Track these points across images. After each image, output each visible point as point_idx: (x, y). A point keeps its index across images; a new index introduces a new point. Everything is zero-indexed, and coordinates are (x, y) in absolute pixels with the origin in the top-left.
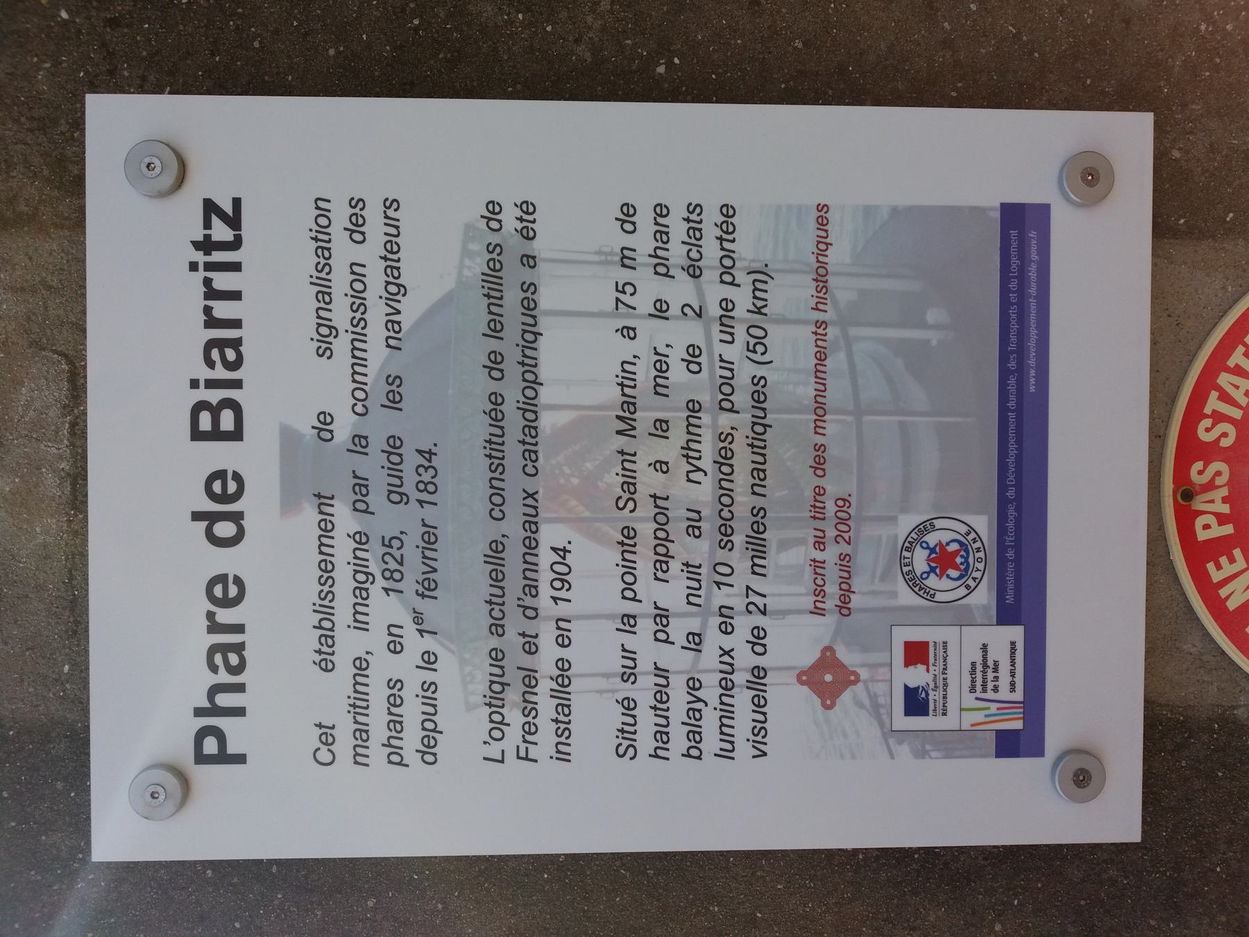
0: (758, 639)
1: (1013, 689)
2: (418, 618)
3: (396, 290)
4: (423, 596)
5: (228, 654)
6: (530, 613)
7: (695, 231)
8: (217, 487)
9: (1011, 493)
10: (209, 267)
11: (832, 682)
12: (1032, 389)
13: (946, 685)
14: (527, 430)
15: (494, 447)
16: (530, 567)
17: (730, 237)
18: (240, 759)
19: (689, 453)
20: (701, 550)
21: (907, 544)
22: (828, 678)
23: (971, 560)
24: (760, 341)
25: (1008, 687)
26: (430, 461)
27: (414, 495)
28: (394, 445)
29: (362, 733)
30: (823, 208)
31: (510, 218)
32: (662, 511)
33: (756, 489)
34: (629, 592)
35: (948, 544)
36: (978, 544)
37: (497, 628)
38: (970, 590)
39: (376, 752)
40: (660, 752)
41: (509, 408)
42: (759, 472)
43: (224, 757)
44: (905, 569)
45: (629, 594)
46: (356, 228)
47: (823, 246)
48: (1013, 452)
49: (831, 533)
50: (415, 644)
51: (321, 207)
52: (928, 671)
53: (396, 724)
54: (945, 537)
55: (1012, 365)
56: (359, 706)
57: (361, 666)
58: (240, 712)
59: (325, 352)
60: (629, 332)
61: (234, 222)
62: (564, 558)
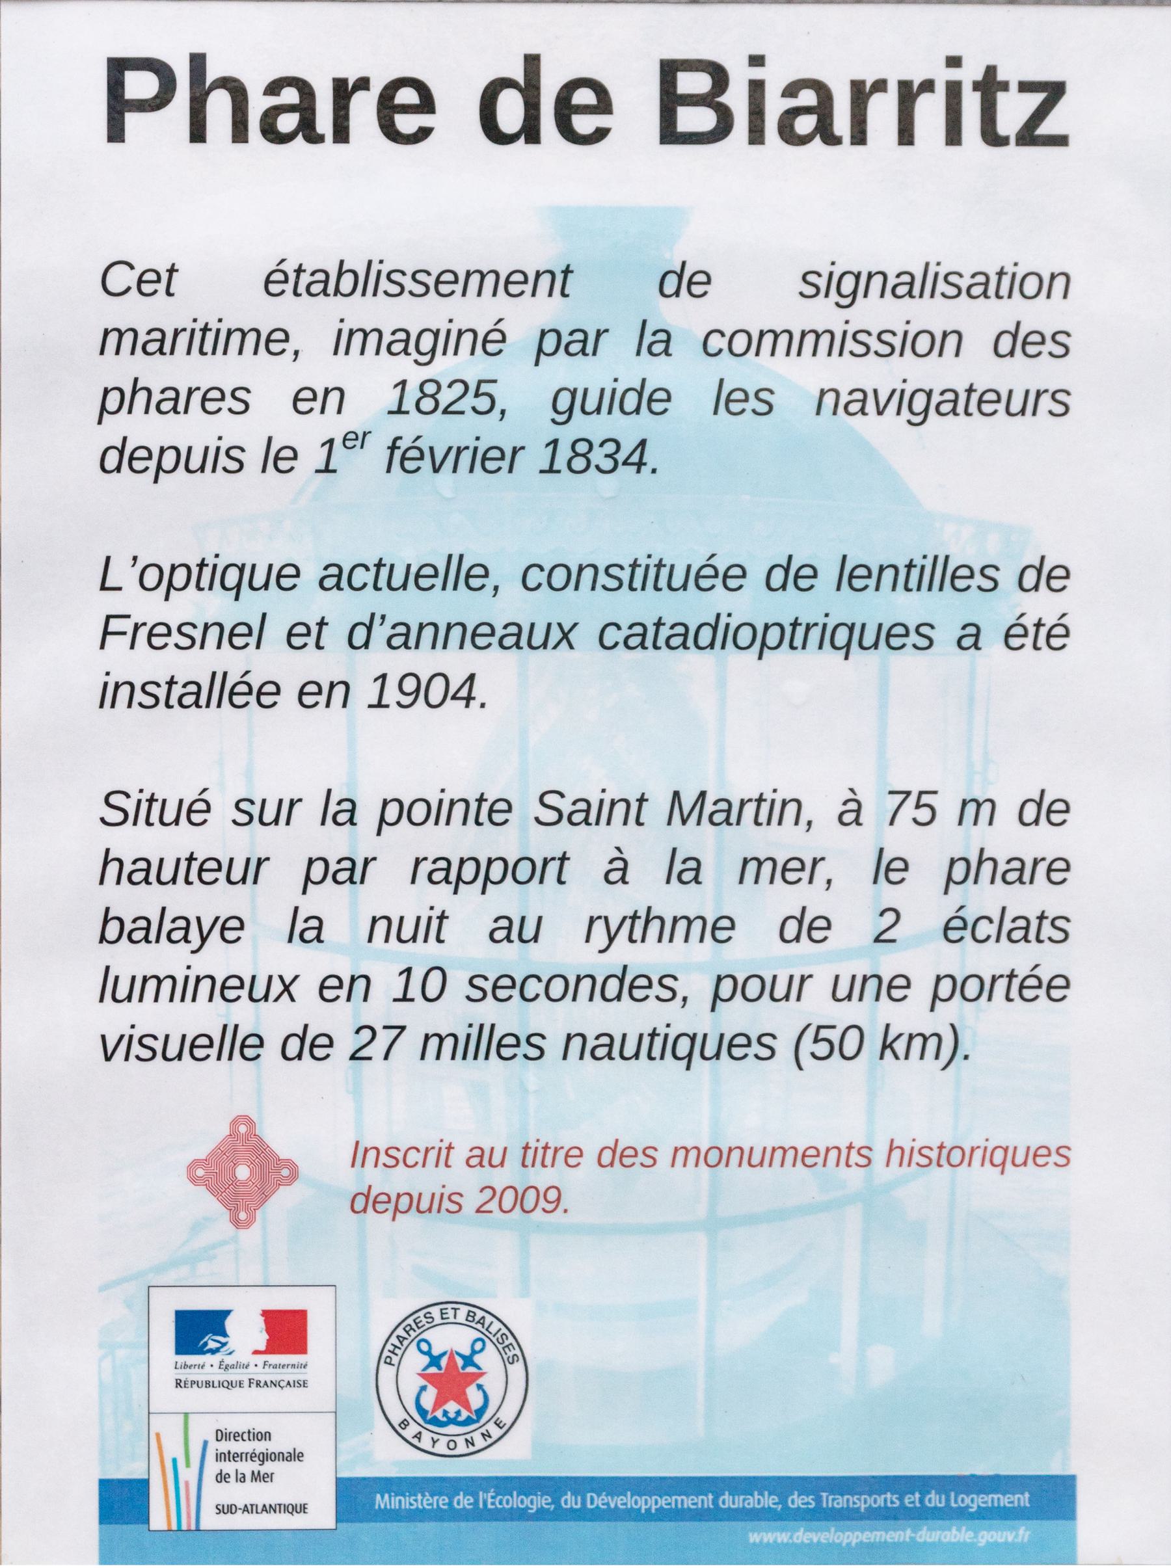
0: (309, 1045)
1: (223, 1510)
2: (355, 439)
3: (920, 407)
4: (393, 448)
5: (301, 114)
6: (360, 636)
7: (1025, 930)
8: (585, 96)
9: (569, 1501)
10: (954, 90)
11: (234, 1181)
12: (754, 1538)
13: (230, 1385)
14: (680, 630)
15: (650, 575)
16: (441, 635)
17: (1014, 993)
18: (116, 133)
19: (641, 923)
20: (467, 945)
21: (480, 1314)
22: (243, 1172)
23: (452, 1429)
24: (836, 1049)
25: (227, 1501)
26: (625, 463)
27: (566, 435)
28: (652, 400)
29: (161, 343)
30: (1063, 1155)
31: (1042, 606)
32: (538, 871)
33: (576, 1043)
34: (398, 812)
35: (480, 1387)
36: (480, 1442)
37: (336, 578)
38: (397, 1429)
39: (122, 369)
40: (113, 868)
41: (719, 601)
42: (608, 1048)
43: (118, 106)
44: (435, 1312)
45: (392, 812)
46: (1018, 342)
47: (1003, 1158)
48: (643, 1503)
49: (500, 1178)
50: (308, 434)
51: (1052, 284)
52: (256, 1352)
53: (174, 402)
54: (493, 1381)
55: (797, 1501)
56: (207, 339)
57: (271, 341)
58: (198, 133)
59: (814, 284)
60: (852, 813)
61: (1028, 136)
62: (454, 698)
